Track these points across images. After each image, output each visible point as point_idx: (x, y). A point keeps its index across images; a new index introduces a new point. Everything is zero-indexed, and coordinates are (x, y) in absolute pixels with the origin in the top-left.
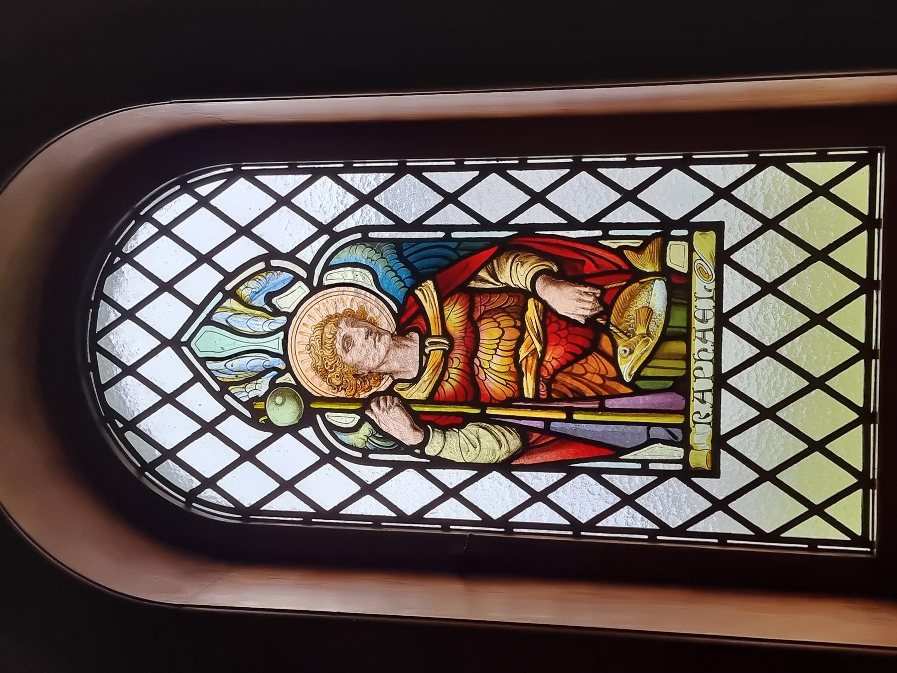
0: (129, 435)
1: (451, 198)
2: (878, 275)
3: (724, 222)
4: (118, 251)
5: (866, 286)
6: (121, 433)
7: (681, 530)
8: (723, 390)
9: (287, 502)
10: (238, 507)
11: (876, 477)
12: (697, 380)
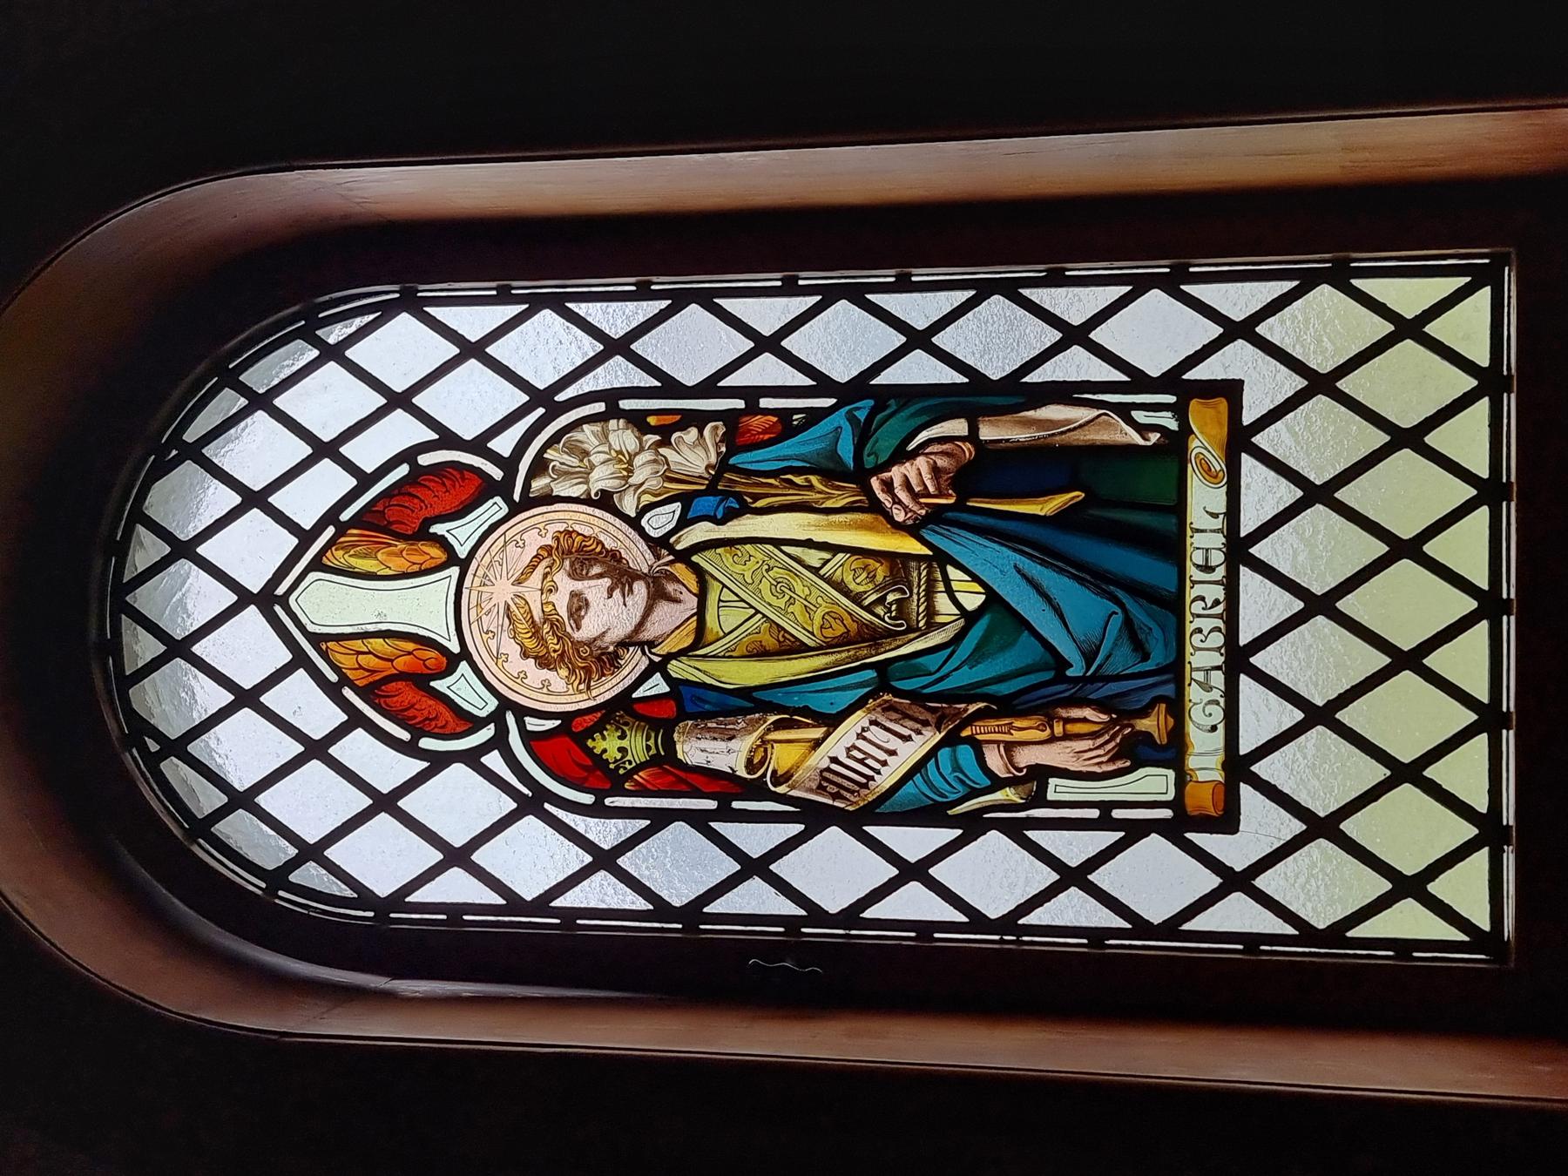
0: (173, 768)
1: (769, 344)
2: (1509, 702)
3: (1243, 381)
5: (1489, 492)
6: (153, 761)
8: (1243, 455)
10: (364, 897)
12: (1196, 586)
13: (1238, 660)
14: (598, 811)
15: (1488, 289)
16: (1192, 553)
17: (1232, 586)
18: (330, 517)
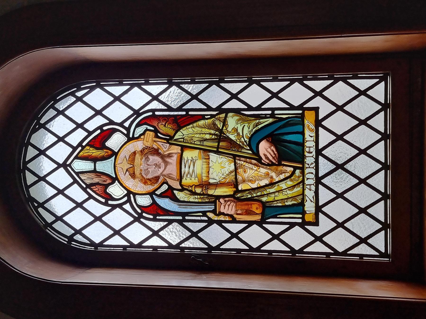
0: (40, 210)
2: (389, 192)
4: (38, 123)
6: (36, 208)
7: (345, 253)
9: (117, 241)
10: (92, 244)
11: (391, 133)
13: (318, 180)
14: (154, 220)
15: (384, 82)
16: (306, 148)
17: (317, 162)
18: (80, 144)
